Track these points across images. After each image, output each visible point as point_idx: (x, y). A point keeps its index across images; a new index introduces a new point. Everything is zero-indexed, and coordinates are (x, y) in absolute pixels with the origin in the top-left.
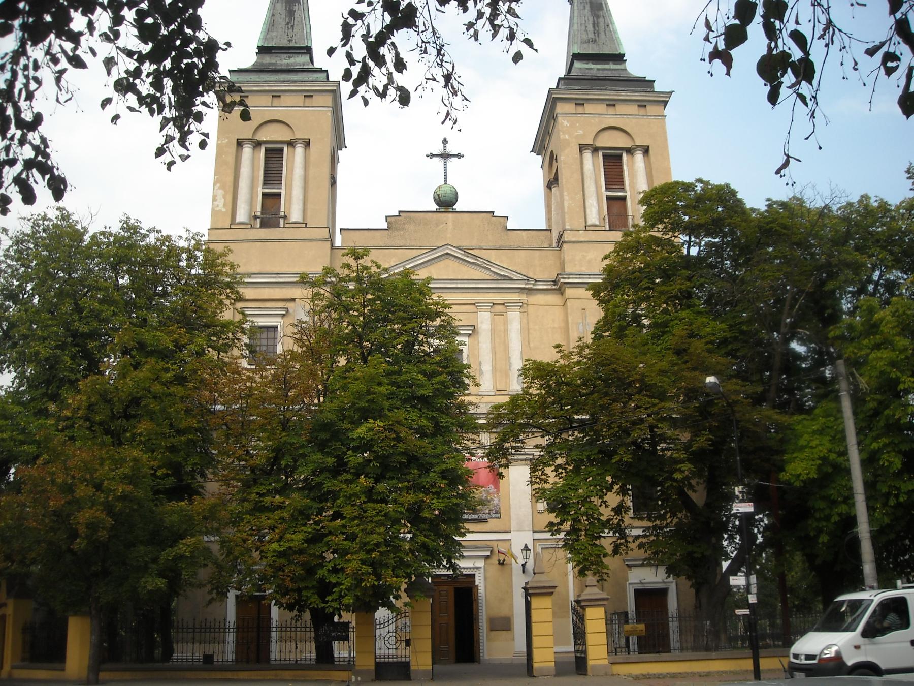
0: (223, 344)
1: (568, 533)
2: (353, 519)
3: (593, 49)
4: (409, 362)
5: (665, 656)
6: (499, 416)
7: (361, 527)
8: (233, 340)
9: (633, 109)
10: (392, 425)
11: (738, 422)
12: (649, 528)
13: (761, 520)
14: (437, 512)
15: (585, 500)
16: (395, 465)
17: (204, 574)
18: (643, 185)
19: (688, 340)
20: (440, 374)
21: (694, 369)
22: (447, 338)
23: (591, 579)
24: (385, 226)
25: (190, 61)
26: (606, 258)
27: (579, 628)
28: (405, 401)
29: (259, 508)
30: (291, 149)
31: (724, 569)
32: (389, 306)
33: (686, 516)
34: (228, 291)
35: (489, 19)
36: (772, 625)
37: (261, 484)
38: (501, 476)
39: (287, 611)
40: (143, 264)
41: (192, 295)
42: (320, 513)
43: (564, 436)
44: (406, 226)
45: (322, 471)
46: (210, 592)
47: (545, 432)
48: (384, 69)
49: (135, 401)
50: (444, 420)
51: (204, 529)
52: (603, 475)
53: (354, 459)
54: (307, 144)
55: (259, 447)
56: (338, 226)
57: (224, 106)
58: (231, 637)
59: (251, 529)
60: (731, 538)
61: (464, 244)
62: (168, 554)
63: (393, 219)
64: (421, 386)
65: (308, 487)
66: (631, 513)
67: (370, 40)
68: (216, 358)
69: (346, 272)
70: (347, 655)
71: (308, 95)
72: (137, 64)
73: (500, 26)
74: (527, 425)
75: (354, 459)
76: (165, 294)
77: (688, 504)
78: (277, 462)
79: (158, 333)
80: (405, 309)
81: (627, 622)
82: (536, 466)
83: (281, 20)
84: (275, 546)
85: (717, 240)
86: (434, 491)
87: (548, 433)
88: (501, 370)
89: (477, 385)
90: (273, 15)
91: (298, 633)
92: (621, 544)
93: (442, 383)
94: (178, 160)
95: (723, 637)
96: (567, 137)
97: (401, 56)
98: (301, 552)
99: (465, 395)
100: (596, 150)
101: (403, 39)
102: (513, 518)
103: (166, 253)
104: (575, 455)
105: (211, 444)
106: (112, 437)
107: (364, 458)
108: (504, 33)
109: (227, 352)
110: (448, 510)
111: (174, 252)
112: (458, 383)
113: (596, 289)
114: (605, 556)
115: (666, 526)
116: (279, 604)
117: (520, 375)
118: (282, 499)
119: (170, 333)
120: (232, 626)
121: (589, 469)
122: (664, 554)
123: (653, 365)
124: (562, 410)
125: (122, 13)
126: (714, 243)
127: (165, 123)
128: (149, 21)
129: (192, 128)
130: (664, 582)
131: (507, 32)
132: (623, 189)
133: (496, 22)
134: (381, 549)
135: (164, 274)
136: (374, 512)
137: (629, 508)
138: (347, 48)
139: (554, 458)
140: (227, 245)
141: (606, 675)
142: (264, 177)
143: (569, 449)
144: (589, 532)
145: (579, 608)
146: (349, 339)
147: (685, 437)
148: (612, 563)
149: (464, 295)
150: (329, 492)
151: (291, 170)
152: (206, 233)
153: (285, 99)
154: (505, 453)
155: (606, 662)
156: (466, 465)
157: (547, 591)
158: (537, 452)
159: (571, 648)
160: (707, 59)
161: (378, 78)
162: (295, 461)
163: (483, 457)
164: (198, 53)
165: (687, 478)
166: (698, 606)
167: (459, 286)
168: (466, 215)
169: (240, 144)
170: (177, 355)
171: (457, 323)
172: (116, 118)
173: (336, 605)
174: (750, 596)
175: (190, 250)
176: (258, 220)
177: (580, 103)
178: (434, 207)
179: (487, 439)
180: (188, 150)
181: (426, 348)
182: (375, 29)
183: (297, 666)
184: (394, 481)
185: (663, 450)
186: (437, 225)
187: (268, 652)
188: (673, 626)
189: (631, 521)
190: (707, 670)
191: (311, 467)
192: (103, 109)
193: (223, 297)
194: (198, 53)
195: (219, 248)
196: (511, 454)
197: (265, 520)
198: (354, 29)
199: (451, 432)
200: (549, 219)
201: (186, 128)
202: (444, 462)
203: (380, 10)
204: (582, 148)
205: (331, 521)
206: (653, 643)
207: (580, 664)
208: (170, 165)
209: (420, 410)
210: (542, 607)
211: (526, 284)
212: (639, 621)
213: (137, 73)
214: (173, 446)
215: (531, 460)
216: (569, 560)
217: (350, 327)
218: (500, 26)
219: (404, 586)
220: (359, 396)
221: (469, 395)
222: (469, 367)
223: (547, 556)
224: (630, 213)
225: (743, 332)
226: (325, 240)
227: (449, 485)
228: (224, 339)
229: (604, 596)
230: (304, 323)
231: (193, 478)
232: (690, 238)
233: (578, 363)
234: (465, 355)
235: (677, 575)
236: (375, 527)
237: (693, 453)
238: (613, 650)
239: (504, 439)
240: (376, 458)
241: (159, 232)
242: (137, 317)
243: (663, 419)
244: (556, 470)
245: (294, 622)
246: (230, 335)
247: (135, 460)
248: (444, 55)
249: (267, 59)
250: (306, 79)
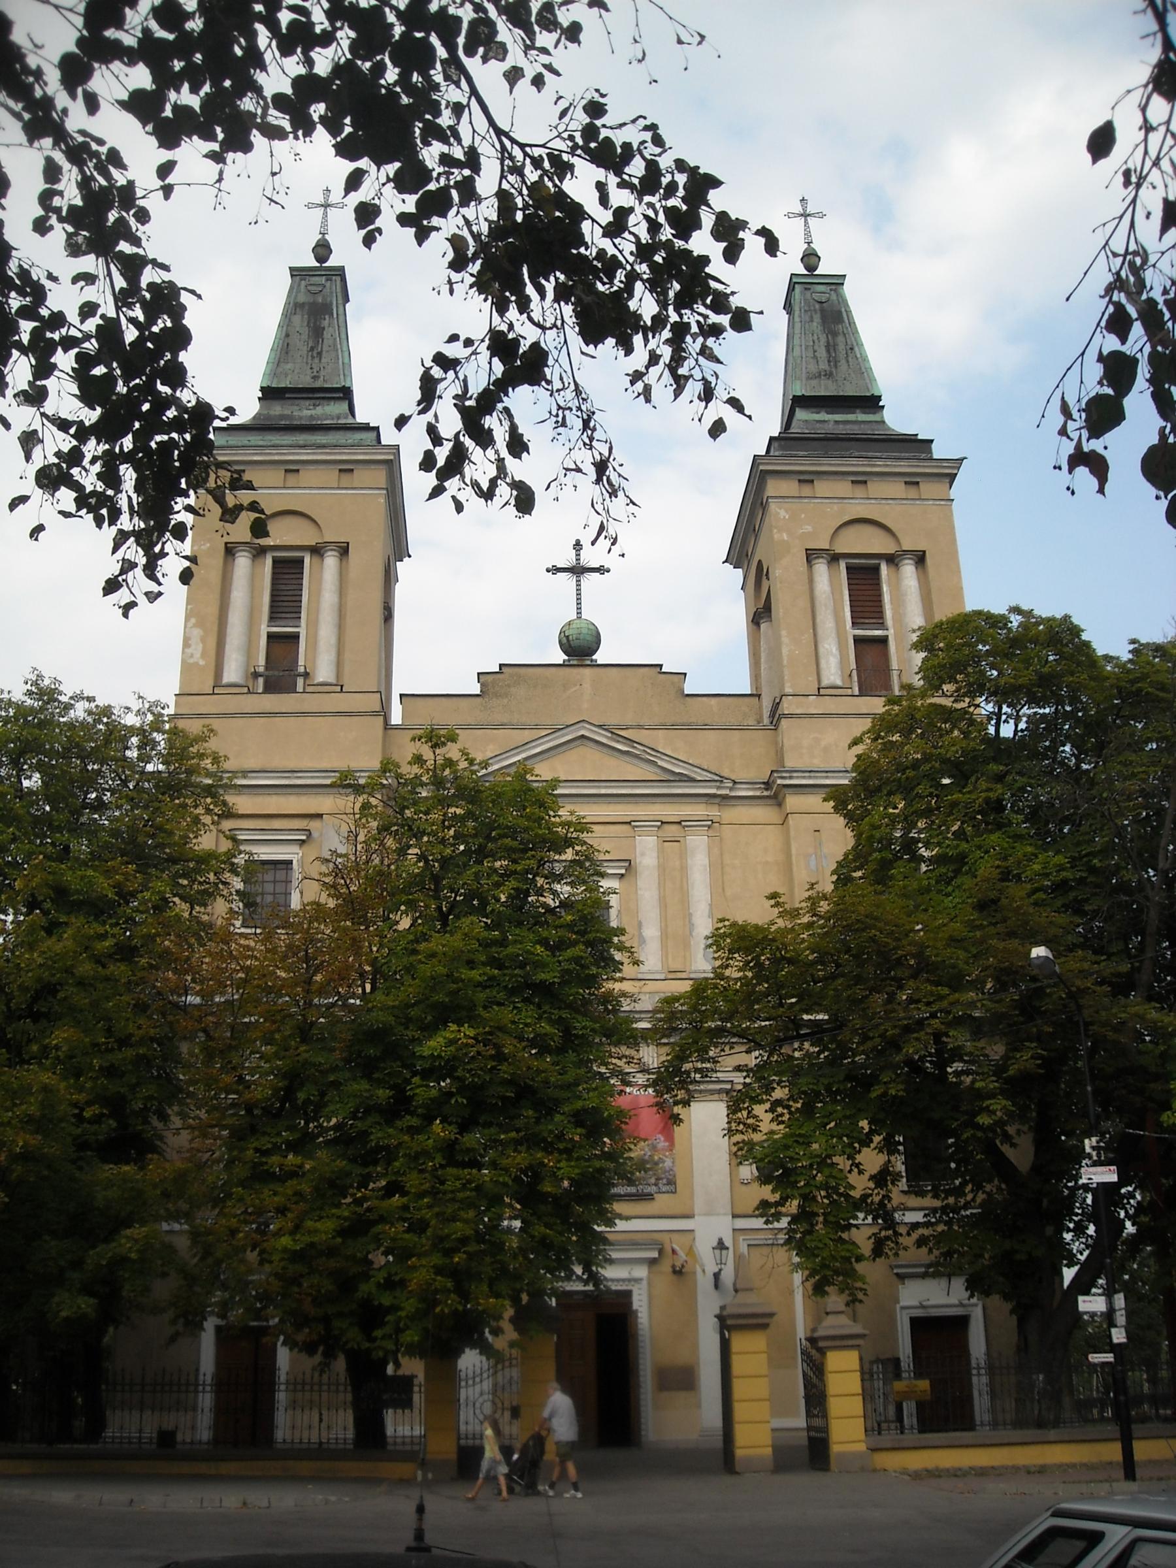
0: (198, 892)
1: (795, 1219)
2: (421, 1195)
3: (826, 388)
4: (520, 924)
5: (967, 1436)
6: (673, 1016)
7: (436, 1210)
8: (216, 884)
9: (897, 489)
10: (490, 1033)
11: (1087, 1024)
12: (934, 1210)
13: (1131, 1195)
14: (566, 1183)
15: (823, 1162)
16: (495, 1101)
17: (163, 1290)
18: (916, 619)
19: (999, 885)
20: (574, 944)
21: (1011, 934)
22: (584, 882)
23: (835, 1299)
24: (476, 689)
25: (166, 437)
26: (855, 742)
27: (815, 1386)
28: (512, 992)
29: (260, 1176)
30: (316, 559)
31: (1066, 1283)
32: (487, 831)
33: (999, 1189)
34: (209, 800)
35: (669, 366)
36: (1153, 1381)
37: (264, 1133)
38: (676, 1119)
39: (304, 1356)
40: (66, 754)
41: (146, 807)
42: (363, 1184)
43: (786, 1050)
44: (513, 690)
45: (368, 1111)
46: (173, 1322)
47: (753, 1041)
48: (490, 453)
49: (48, 990)
50: (580, 1024)
51: (162, 1212)
52: (854, 1118)
53: (424, 1091)
54: (344, 551)
55: (260, 1073)
56: (397, 689)
57: (223, 514)
58: (206, 1400)
59: (245, 1212)
60: (1080, 1230)
61: (612, 720)
62: (99, 1255)
63: (490, 678)
64: (540, 965)
65: (344, 1139)
66: (903, 1184)
67: (468, 403)
68: (186, 915)
69: (416, 769)
70: (408, 1433)
71: (346, 469)
72: (75, 443)
73: (687, 378)
74: (720, 1031)
75: (424, 1091)
76: (99, 806)
77: (1003, 1168)
78: (294, 1097)
79: (90, 872)
80: (512, 832)
81: (898, 1376)
82: (738, 1102)
83: (301, 345)
84: (285, 1241)
85: (1047, 710)
86: (561, 1146)
87: (758, 1046)
88: (675, 936)
89: (637, 963)
90: (287, 335)
91: (325, 1395)
92: (887, 1238)
93: (577, 960)
94: (142, 600)
95: (1067, 1401)
96: (785, 537)
97: (520, 431)
98: (331, 1252)
99: (616, 980)
100: (834, 558)
101: (524, 402)
102: (698, 1194)
103: (103, 737)
104: (804, 1083)
105: (177, 1062)
106: (8, 1052)
107: (441, 1089)
108: (693, 388)
109: (205, 905)
110: (582, 1173)
111: (116, 734)
112: (604, 959)
113: (839, 798)
114: (859, 1259)
115: (966, 1206)
116: (290, 1343)
117: (710, 946)
118: (299, 1160)
119: (108, 873)
120: (209, 1380)
121: (830, 1108)
122: (962, 1255)
123: (939, 927)
124: (781, 1005)
125: (52, 360)
126: (1044, 715)
127: (121, 539)
128: (99, 371)
129: (168, 548)
130: (961, 1305)
131: (699, 387)
132: (882, 625)
133: (681, 371)
134: (469, 1249)
135: (100, 771)
136: (458, 1184)
137: (899, 1174)
138: (429, 417)
139: (769, 1089)
140: (207, 721)
141: (863, 1469)
142: (271, 607)
143: (793, 1071)
144: (831, 1219)
145: (814, 1352)
146: (416, 882)
147: (997, 1050)
148: (872, 1272)
149: (612, 807)
150: (379, 1149)
151: (317, 593)
152: (171, 701)
153: (308, 476)
154: (685, 1082)
155: (862, 1447)
156: (621, 1102)
157: (758, 1322)
158: (739, 1079)
159: (801, 1422)
160: (1065, 467)
161: (480, 466)
162: (323, 1094)
163: (646, 1086)
164: (177, 425)
165: (1000, 1123)
166: (1023, 1347)
167: (603, 791)
168: (614, 669)
170: (120, 911)
171: (602, 857)
172: (37, 530)
173: (390, 1346)
174: (1113, 1331)
175: (145, 731)
176: (261, 680)
177: (807, 479)
178: (560, 657)
179: (652, 1056)
180: (160, 584)
181: (549, 900)
182: (477, 386)
183: (320, 1452)
184: (493, 1130)
185: (957, 1074)
187: (270, 1426)
188: (980, 1382)
189: (904, 1199)
190: (1041, 1461)
191: (351, 1107)
192: (11, 510)
193: (200, 810)
194: (177, 425)
195: (193, 727)
196: (695, 1082)
197: (270, 1196)
198: (441, 387)
199: (591, 1044)
200: (756, 677)
201: (157, 549)
202: (579, 1098)
203: (485, 354)
204: (811, 555)
205: (383, 1198)
206: (945, 1414)
207: (815, 1451)
208: (127, 608)
209: (539, 1006)
210: (750, 1351)
211: (718, 788)
212: (919, 1375)
213: (74, 457)
214: (112, 1066)
215: (727, 1092)
216: (797, 1267)
217: (421, 864)
218: (687, 378)
219: (509, 1312)
220: (435, 983)
221: (622, 979)
222: (621, 931)
223: (757, 1259)
224: (894, 665)
225: (1092, 870)
226: (374, 714)
227: (588, 1136)
228: (200, 883)
229: (857, 1329)
230: (341, 856)
231: (146, 1122)
232: (1000, 708)
233: (810, 925)
234: (613, 913)
235: (987, 1293)
236: (459, 1209)
237: (1008, 1081)
238: (874, 1427)
239: (681, 1057)
240: (461, 1090)
241: (91, 699)
242: (53, 844)
243: (958, 1022)
244: (772, 1110)
245: (316, 1375)
246: (212, 876)
247: (45, 1089)
248: (594, 430)
249: (277, 409)
250: (343, 442)
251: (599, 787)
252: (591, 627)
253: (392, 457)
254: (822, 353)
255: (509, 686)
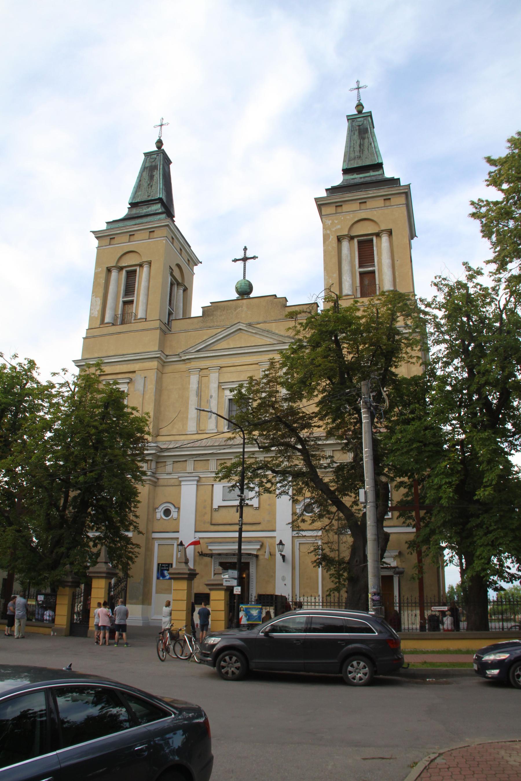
9: (380, 202)
30: (379, 239)
54: (390, 233)
90: (140, 181)
100: (352, 238)
132: (373, 266)
167: (246, 351)
169: (109, 270)
186: (236, 309)
249: (135, 211)
251: (244, 350)
252: (247, 282)
253: (406, 191)
254: (357, 148)
255: (213, 311)
